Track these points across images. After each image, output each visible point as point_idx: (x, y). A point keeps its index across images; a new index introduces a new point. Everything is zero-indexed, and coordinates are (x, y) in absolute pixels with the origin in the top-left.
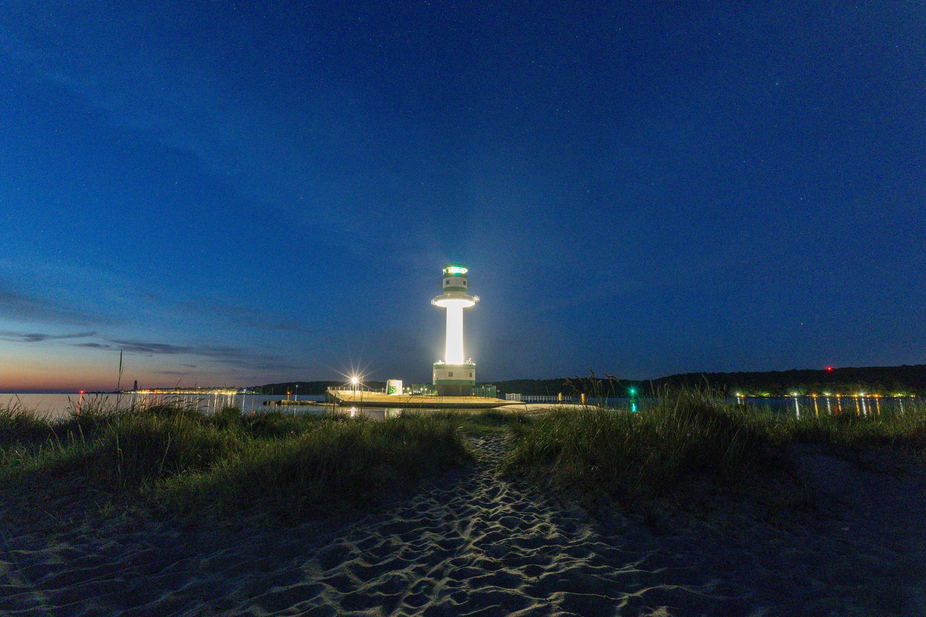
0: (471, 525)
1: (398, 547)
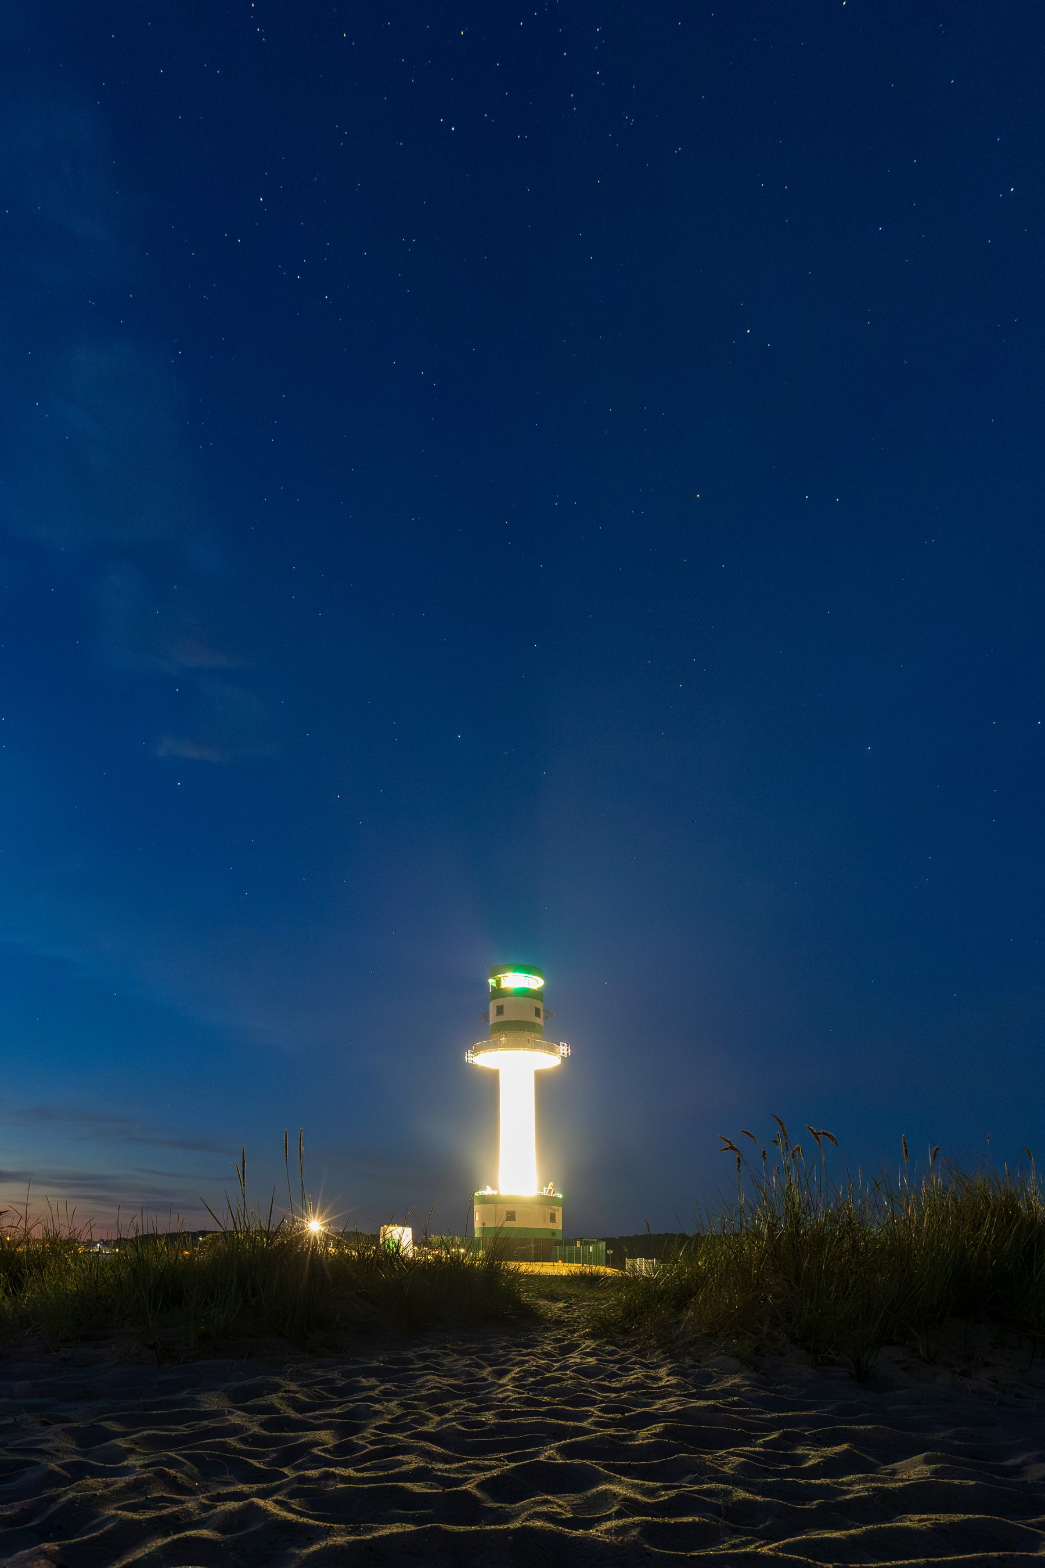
1: (372, 1388)
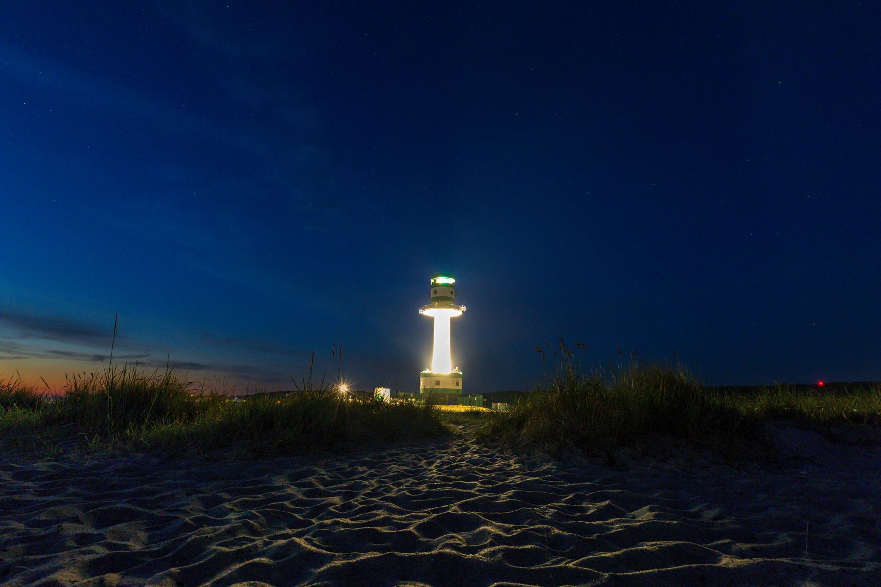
1: (364, 472)
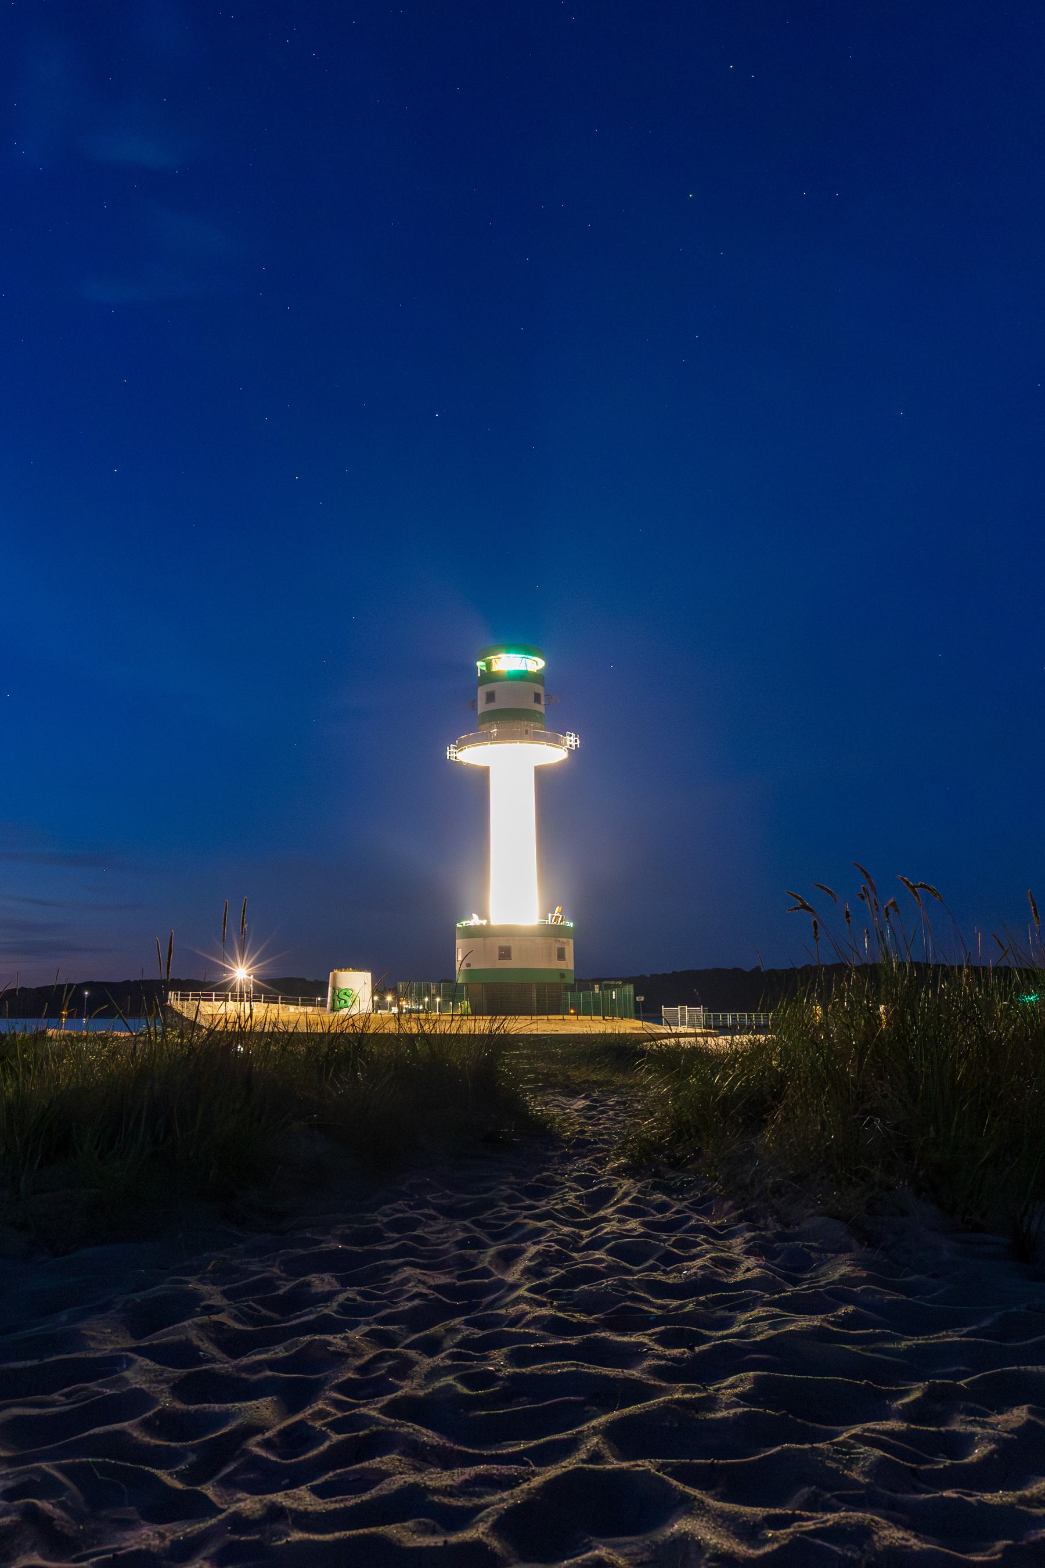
0: (529, 1254)
1: (329, 1297)
